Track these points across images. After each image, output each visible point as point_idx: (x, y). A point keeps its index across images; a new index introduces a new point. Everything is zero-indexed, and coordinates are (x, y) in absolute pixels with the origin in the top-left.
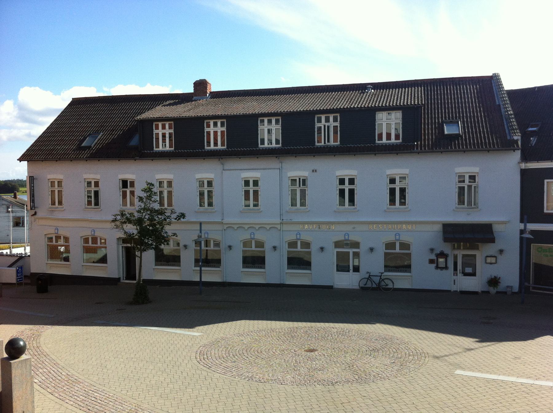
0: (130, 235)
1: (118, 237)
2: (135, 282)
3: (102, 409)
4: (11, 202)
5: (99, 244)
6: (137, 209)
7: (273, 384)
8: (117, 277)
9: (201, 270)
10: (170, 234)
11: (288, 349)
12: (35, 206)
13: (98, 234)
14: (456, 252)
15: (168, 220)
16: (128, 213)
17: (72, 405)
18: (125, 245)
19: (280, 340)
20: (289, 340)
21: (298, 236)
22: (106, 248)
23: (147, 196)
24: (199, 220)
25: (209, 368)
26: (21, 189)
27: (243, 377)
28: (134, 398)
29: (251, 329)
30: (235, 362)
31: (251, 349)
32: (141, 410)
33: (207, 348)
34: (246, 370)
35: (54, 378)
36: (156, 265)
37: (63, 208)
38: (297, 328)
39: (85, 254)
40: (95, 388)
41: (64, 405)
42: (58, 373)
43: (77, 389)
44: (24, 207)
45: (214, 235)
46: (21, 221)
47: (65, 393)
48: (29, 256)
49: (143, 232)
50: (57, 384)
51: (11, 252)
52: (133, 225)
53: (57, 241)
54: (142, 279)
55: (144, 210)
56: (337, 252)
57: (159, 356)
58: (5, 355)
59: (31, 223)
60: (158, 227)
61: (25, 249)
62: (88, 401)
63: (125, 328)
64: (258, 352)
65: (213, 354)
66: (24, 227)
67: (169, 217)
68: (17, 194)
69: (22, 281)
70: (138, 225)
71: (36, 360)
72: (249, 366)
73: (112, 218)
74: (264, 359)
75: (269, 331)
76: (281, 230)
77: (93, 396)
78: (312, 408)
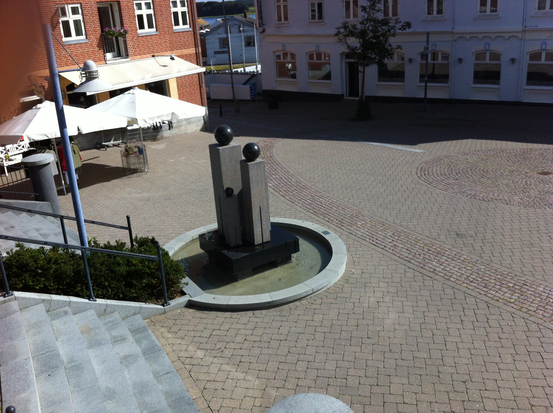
0: (353, 50)
1: (341, 52)
2: (357, 98)
3: (327, 213)
4: (241, 22)
5: (323, 61)
6: (360, 21)
7: (498, 204)
8: (340, 94)
9: (426, 86)
10: (395, 47)
11: (518, 170)
12: (263, 23)
13: (323, 49)
15: (392, 31)
16: (351, 25)
17: (300, 207)
18: (348, 60)
19: (510, 161)
20: (520, 162)
21: (544, 46)
22: (329, 64)
23: (371, 5)
24: (426, 30)
25: (430, 183)
26: (250, 9)
27: (465, 195)
28: (355, 205)
29: (478, 149)
30: (457, 179)
31: (476, 168)
32: (361, 216)
33: (428, 164)
34: (469, 188)
35: (285, 184)
36: (379, 81)
37: (289, 23)
38: (531, 149)
39: (310, 72)
40: (320, 194)
41: (294, 206)
42: (288, 179)
43: (304, 194)
44: (254, 26)
45: (443, 47)
46: (252, 40)
47: (295, 197)
48: (260, 74)
49: (366, 45)
50: (288, 189)
51: (244, 70)
52: (356, 38)
53: (284, 58)
54: (365, 95)
55: (367, 22)
57: (379, 170)
58: (244, 158)
59: (260, 41)
60: (382, 39)
61: (257, 68)
62: (314, 205)
63: (348, 142)
64: (484, 172)
65: (434, 170)
66: (255, 46)
67: (393, 27)
68: (247, 14)
69: (255, 98)
70: (361, 38)
71: (270, 167)
72: (473, 184)
73: (334, 31)
74: (490, 179)
75: (498, 151)
76: (523, 39)
77: (318, 201)
78: (539, 230)
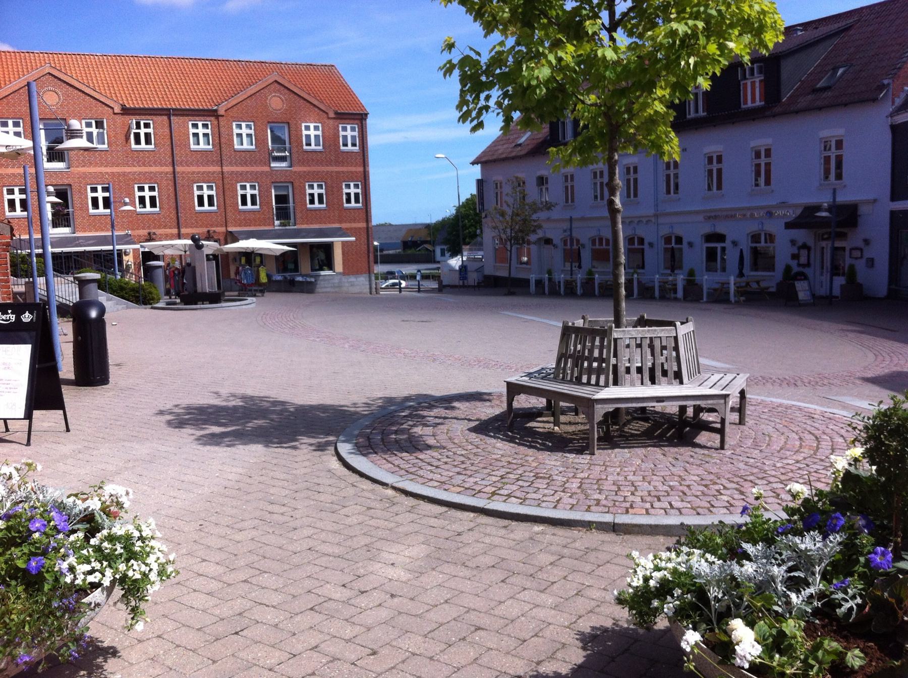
14: (824, 244)
56: (707, 248)
